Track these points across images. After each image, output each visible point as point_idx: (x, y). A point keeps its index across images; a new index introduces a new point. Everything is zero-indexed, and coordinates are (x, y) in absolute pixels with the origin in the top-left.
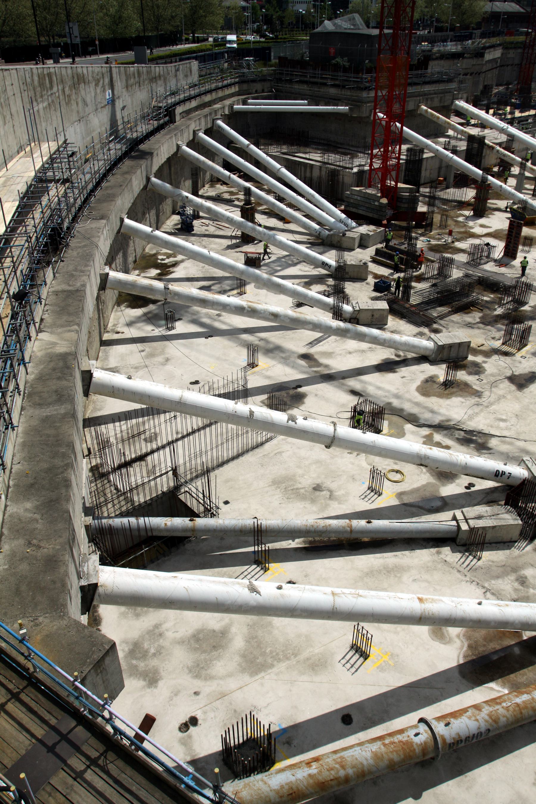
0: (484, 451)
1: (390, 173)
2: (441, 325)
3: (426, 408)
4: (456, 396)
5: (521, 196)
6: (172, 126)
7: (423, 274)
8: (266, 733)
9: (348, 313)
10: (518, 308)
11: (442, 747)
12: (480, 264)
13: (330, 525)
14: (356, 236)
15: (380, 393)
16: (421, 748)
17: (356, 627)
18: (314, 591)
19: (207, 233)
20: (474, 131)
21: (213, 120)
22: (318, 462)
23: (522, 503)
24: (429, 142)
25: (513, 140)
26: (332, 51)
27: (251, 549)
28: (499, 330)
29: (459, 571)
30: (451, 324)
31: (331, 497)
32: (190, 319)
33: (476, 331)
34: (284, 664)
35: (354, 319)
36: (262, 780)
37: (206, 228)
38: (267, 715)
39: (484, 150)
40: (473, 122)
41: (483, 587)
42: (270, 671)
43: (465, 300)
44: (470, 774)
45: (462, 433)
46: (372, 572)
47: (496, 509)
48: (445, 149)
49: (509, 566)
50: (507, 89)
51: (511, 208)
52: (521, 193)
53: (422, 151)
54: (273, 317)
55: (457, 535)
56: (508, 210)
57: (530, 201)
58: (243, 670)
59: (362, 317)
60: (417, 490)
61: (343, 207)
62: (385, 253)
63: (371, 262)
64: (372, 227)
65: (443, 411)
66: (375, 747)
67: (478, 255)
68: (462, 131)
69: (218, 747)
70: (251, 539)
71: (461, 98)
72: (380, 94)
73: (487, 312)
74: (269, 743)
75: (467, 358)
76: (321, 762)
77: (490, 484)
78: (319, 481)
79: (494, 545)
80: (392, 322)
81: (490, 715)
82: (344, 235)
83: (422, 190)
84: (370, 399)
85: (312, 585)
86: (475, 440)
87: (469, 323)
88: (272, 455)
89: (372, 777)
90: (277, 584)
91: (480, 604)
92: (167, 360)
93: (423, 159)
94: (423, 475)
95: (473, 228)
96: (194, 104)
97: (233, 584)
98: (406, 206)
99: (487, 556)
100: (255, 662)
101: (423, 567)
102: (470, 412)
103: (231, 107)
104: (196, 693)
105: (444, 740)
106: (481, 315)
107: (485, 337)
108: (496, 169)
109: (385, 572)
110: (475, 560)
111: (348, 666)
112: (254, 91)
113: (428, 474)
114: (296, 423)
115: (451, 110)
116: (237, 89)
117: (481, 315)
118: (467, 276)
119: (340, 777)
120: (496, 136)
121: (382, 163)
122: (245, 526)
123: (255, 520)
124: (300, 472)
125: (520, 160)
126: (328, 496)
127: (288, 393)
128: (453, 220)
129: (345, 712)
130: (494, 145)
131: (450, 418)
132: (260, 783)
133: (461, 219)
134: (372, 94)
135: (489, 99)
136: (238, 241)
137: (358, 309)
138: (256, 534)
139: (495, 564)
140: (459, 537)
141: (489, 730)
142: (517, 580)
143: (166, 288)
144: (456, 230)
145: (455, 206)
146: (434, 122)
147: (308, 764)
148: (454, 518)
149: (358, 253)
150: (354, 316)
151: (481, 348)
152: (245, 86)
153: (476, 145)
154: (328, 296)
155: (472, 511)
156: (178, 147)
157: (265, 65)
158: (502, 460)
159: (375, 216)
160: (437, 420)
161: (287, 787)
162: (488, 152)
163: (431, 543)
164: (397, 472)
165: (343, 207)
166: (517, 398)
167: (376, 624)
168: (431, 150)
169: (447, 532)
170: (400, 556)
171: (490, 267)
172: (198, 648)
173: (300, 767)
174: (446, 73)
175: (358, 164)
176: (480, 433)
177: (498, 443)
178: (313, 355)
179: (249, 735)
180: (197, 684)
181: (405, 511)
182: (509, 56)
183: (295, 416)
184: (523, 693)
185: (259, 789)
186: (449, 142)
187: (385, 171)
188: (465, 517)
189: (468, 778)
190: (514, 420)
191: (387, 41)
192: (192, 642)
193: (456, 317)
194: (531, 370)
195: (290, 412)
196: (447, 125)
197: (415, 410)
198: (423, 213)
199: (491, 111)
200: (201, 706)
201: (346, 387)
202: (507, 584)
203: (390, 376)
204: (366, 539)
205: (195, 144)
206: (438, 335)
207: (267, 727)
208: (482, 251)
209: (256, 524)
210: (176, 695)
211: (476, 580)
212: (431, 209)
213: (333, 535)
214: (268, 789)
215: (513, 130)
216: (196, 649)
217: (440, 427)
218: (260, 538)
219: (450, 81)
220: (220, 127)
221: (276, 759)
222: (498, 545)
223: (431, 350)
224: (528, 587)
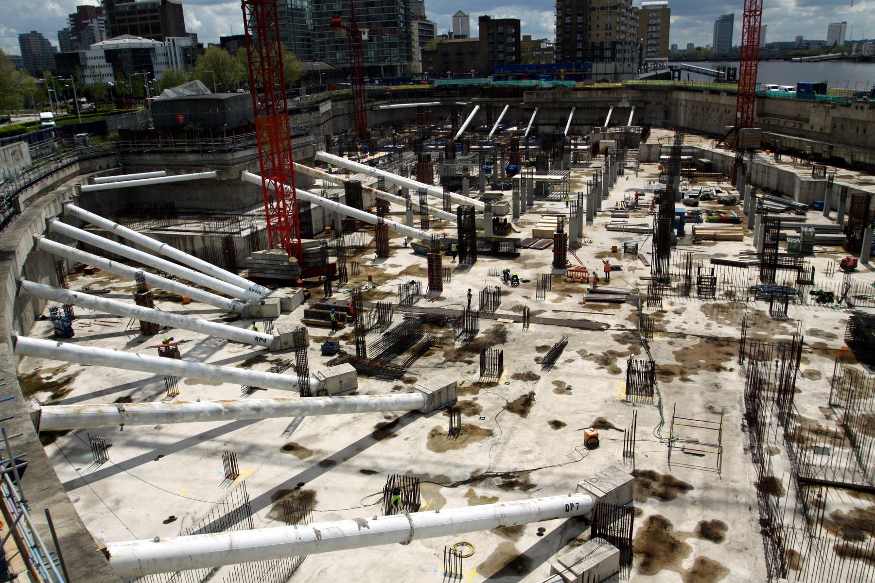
3: (449, 464)
4: (471, 442)
6: (19, 218)
19: (93, 334)
21: (63, 205)
22: (373, 565)
26: (181, 118)
30: (421, 370)
32: (123, 442)
37: (89, 328)
40: (333, 170)
54: (255, 412)
59: (330, 387)
62: (316, 313)
64: (289, 290)
65: (467, 462)
68: (336, 179)
73: (448, 348)
75: (456, 400)
77: (557, 523)
80: (363, 384)
82: (263, 303)
86: (513, 482)
87: (438, 364)
88: (315, 577)
92: (118, 502)
94: (489, 538)
96: (36, 189)
102: (493, 454)
103: (78, 187)
112: (98, 168)
116: (78, 168)
127: (292, 497)
133: (368, 263)
136: (137, 335)
137: (323, 379)
143: (121, 411)
148: (554, 572)
150: (321, 387)
152: (86, 164)
156: (36, 240)
157: (103, 139)
159: (287, 277)
176: (515, 472)
178: (297, 444)
182: (339, 107)
188: (565, 566)
190: (537, 448)
193: (421, 361)
203: (392, 441)
205: (50, 233)
215: (379, 172)
219: (307, 134)
220: (72, 211)
223: (421, 402)
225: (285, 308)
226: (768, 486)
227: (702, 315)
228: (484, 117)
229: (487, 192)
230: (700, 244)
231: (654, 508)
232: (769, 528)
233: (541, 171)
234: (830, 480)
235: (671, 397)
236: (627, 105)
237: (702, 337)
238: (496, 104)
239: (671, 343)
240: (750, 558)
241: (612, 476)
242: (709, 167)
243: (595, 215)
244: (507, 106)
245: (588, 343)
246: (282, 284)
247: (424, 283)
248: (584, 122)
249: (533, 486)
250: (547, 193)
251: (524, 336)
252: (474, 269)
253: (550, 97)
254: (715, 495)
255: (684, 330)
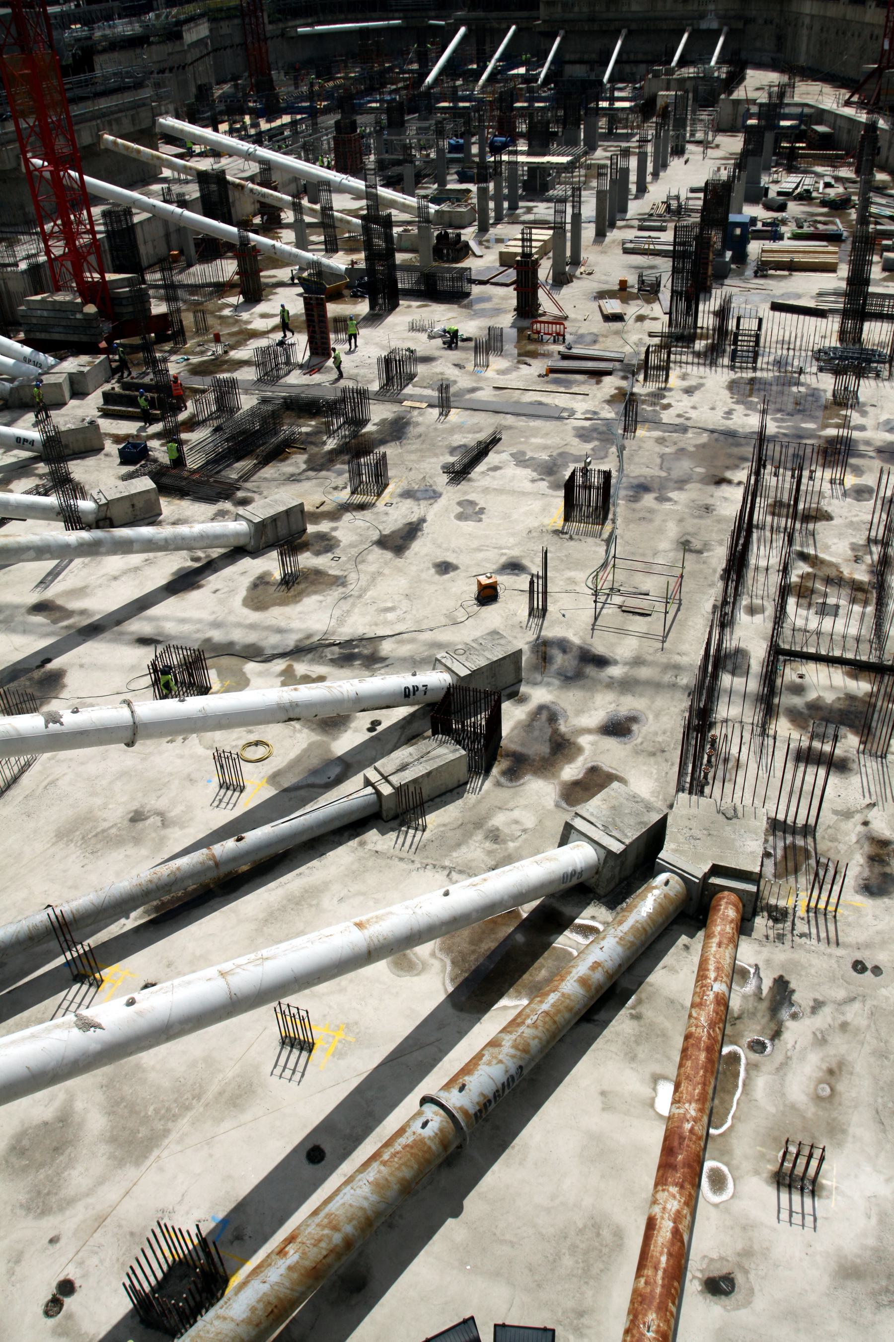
0: (377, 666)
1: (86, 260)
2: (248, 490)
4: (309, 595)
5: (309, 255)
7: (193, 416)
8: (196, 1241)
9: (91, 513)
10: (358, 432)
11: (467, 1126)
12: (279, 377)
13: (178, 869)
14: (61, 380)
15: (186, 628)
16: (437, 1141)
17: (278, 1010)
18: (189, 983)
20: (205, 164)
22: (124, 774)
23: (457, 722)
24: (135, 195)
25: (269, 169)
27: (60, 961)
28: (340, 473)
29: (401, 859)
30: (265, 484)
31: (165, 823)
33: (306, 485)
34: (185, 1120)
35: (104, 519)
36: (218, 1317)
38: (187, 1213)
39: (230, 193)
40: (197, 149)
41: (444, 868)
42: (167, 1141)
43: (274, 441)
44: (517, 1141)
45: (336, 649)
46: (271, 914)
47: (423, 745)
48: (165, 201)
49: (470, 822)
50: (236, 86)
51: (299, 279)
52: (308, 251)
53: (128, 213)
55: (381, 806)
56: (296, 281)
57: (325, 261)
58: (120, 1163)
60: (298, 760)
61: (22, 335)
63: (100, 417)
64: (84, 359)
65: (296, 624)
66: (372, 1174)
67: (272, 366)
68: (185, 167)
69: (123, 1305)
70: (54, 944)
71: (167, 113)
72: (25, 126)
73: (314, 450)
74: (208, 1254)
76: (299, 1240)
77: (402, 712)
78: (135, 806)
79: (438, 800)
80: (169, 507)
81: (515, 1046)
83: (149, 277)
84: (175, 643)
85: (184, 975)
86: (358, 653)
87: (292, 475)
89: (383, 1219)
90: (125, 999)
91: (446, 894)
93: (133, 225)
94: (298, 735)
95: (250, 322)
97: (49, 1031)
98: (130, 309)
99: (434, 820)
100: (135, 1141)
101: (346, 876)
102: (337, 613)
104: (53, 1241)
105: (465, 1112)
106: (305, 457)
107: (322, 489)
108: (257, 220)
109: (292, 906)
110: (419, 833)
111: (288, 1073)
113: (306, 731)
114: (62, 724)
115: (156, 134)
117: (305, 457)
118: (264, 401)
119: (336, 1246)
120: (241, 167)
121: (66, 245)
122: (35, 927)
123: (50, 911)
124: (98, 801)
125: (290, 198)
126: (159, 824)
128: (216, 316)
129: (309, 1146)
130: (243, 182)
131: (310, 631)
132: (216, 1323)
133: (227, 312)
134: (11, 127)
135: (212, 107)
137: (104, 501)
138: (59, 933)
139: (449, 827)
140: (384, 808)
141: (521, 1067)
142: (486, 838)
144: (224, 331)
145: (211, 293)
146: (135, 160)
147: (281, 1252)
148: (368, 783)
149: (73, 407)
151: (322, 509)
153: (214, 187)
154: (46, 494)
155: (388, 763)
158: (407, 670)
159: (84, 338)
160: (290, 641)
161: (261, 1306)
162: (237, 194)
163: (346, 834)
164: (257, 743)
165: (22, 335)
166: (399, 570)
167: (307, 991)
168: (144, 208)
169: (364, 807)
170: (307, 871)
171: (297, 378)
172: (27, 1166)
173: (270, 1265)
174: (127, 72)
175: (24, 254)
176: (362, 639)
177: (394, 646)
178: (52, 602)
179: (170, 1259)
180: (49, 1225)
181: (290, 799)
183: (57, 713)
184: (547, 994)
185: (218, 1334)
186: (169, 188)
187: (76, 257)
188: (382, 775)
189: (517, 1148)
190: (405, 605)
191: (8, 29)
192: (13, 1160)
193: (268, 472)
194: (405, 521)
195: (45, 709)
196: (157, 162)
197: (252, 638)
198: (163, 316)
199: (224, 127)
200: (70, 1256)
201: (126, 637)
202: (475, 850)
203: (194, 596)
204: (245, 868)
206: (249, 508)
207: (193, 1232)
208: (276, 357)
209: (53, 917)
210: (18, 1261)
211: (430, 861)
212: (174, 306)
213: (190, 882)
214: (232, 1326)
216: (24, 1170)
217: (299, 651)
218: (68, 937)
219: (138, 85)
221: (228, 1272)
222: (443, 798)
223: (245, 535)
224: (504, 842)
225: (78, 388)
226: (719, 661)
227: (726, 394)
228: (472, 50)
229: (449, 187)
230: (765, 276)
231: (550, 692)
232: (700, 722)
233: (537, 149)
234: (823, 652)
235: (632, 526)
236: (715, 25)
237: (712, 431)
238: (495, 25)
239: (661, 441)
240: (664, 764)
241: (489, 645)
242: (826, 141)
243: (612, 226)
244: (513, 28)
245: (533, 440)
246: (78, 349)
247: (300, 343)
248: (640, 57)
249: (384, 659)
250: (545, 187)
251: (436, 429)
252: (391, 319)
253: (585, 9)
254: (644, 673)
255: (688, 419)
